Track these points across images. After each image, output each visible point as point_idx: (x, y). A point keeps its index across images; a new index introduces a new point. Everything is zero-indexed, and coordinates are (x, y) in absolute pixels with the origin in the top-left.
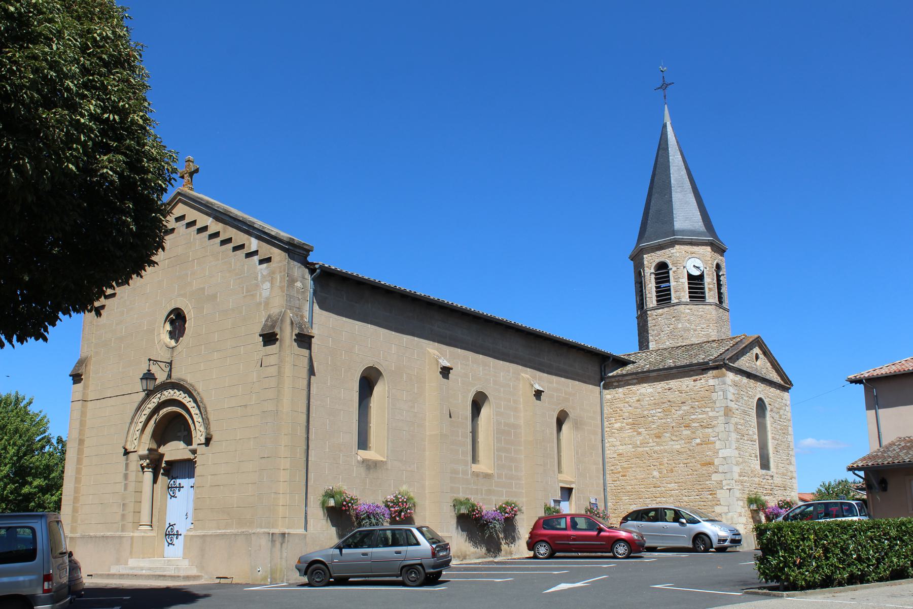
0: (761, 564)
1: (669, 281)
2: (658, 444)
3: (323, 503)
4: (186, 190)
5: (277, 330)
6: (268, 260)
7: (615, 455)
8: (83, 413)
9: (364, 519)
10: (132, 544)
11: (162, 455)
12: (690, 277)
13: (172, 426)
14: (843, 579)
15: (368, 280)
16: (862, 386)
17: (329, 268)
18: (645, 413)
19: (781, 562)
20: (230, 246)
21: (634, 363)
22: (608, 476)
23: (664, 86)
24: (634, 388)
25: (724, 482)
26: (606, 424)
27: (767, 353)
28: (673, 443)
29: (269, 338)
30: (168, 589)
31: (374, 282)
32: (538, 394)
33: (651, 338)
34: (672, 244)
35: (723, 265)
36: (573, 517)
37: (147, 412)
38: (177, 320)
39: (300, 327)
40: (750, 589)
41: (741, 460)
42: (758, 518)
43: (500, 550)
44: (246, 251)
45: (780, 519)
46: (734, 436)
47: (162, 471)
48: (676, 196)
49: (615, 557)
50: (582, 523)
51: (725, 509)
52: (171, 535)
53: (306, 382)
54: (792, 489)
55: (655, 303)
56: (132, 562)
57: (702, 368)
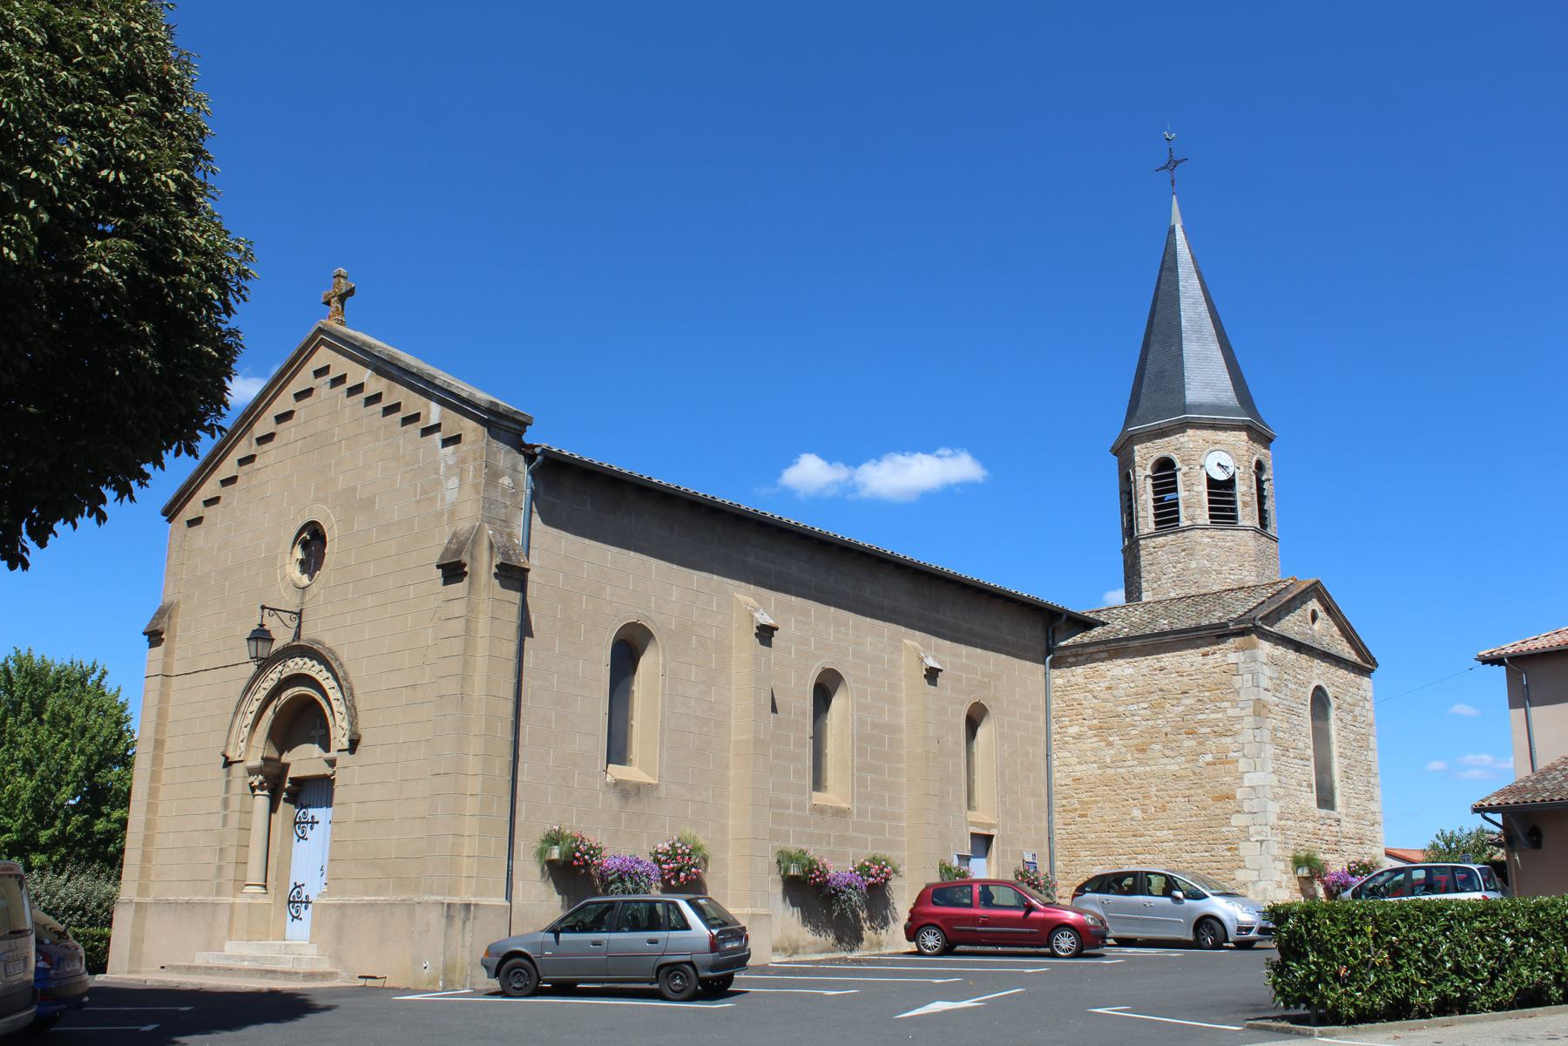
0: (1279, 975)
1: (1175, 490)
2: (1141, 763)
3: (542, 853)
4: (333, 325)
5: (465, 558)
6: (455, 440)
8: (163, 697)
9: (612, 882)
10: (231, 917)
11: (286, 767)
12: (1212, 483)
13: (300, 720)
14: (1427, 1005)
15: (630, 476)
16: (1503, 668)
17: (559, 454)
18: (1121, 709)
19: (1311, 972)
20: (398, 416)
21: (1104, 624)
22: (1056, 816)
23: (1172, 164)
24: (1102, 666)
25: (1252, 830)
26: (1054, 727)
27: (1331, 609)
28: (1165, 761)
29: (453, 571)
30: (274, 994)
31: (640, 479)
32: (932, 675)
33: (1144, 585)
34: (1182, 427)
35: (1268, 464)
36: (986, 885)
37: (261, 695)
38: (313, 540)
39: (506, 554)
40: (1257, 1017)
41: (1282, 791)
42: (1311, 891)
43: (860, 939)
44: (422, 424)
45: (1349, 893)
46: (1270, 750)
47: (284, 795)
48: (1189, 348)
49: (1053, 955)
50: (1002, 896)
51: (1253, 875)
52: (296, 902)
53: (512, 648)
54: (1373, 842)
55: (1152, 526)
56: (231, 948)
57: (1218, 634)
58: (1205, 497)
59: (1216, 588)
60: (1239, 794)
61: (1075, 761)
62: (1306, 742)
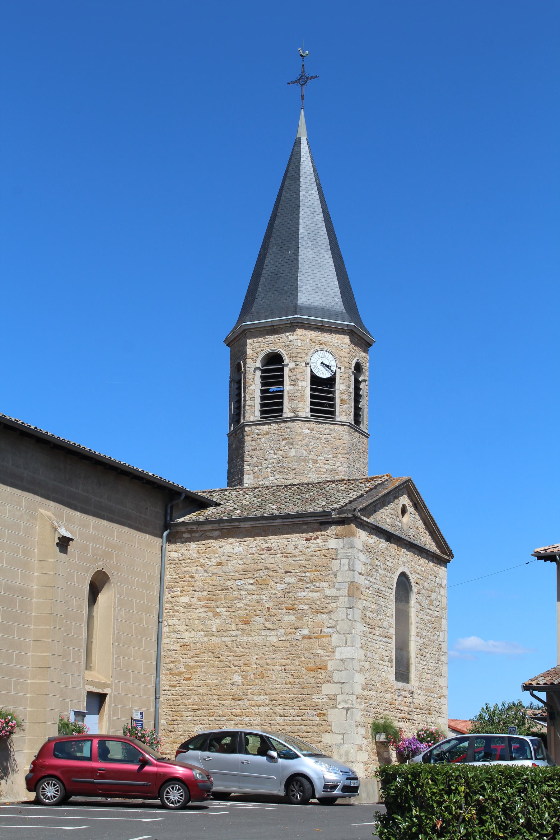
0: (385, 826)
1: (281, 383)
2: (244, 633)
7: (177, 646)
12: (315, 380)
16: (554, 564)
18: (229, 583)
19: (413, 824)
21: (217, 504)
22: (163, 678)
23: (303, 80)
24: (215, 544)
25: (340, 698)
26: (167, 596)
27: (419, 505)
28: (267, 632)
32: (64, 543)
33: (247, 468)
34: (292, 326)
35: (366, 366)
36: (103, 740)
41: (367, 665)
42: (385, 755)
45: (419, 758)
46: (359, 628)
49: (163, 806)
50: (116, 750)
51: (338, 739)
55: (258, 414)
57: (321, 521)
58: (308, 392)
59: (314, 478)
60: (331, 665)
61: (184, 629)
62: (389, 622)
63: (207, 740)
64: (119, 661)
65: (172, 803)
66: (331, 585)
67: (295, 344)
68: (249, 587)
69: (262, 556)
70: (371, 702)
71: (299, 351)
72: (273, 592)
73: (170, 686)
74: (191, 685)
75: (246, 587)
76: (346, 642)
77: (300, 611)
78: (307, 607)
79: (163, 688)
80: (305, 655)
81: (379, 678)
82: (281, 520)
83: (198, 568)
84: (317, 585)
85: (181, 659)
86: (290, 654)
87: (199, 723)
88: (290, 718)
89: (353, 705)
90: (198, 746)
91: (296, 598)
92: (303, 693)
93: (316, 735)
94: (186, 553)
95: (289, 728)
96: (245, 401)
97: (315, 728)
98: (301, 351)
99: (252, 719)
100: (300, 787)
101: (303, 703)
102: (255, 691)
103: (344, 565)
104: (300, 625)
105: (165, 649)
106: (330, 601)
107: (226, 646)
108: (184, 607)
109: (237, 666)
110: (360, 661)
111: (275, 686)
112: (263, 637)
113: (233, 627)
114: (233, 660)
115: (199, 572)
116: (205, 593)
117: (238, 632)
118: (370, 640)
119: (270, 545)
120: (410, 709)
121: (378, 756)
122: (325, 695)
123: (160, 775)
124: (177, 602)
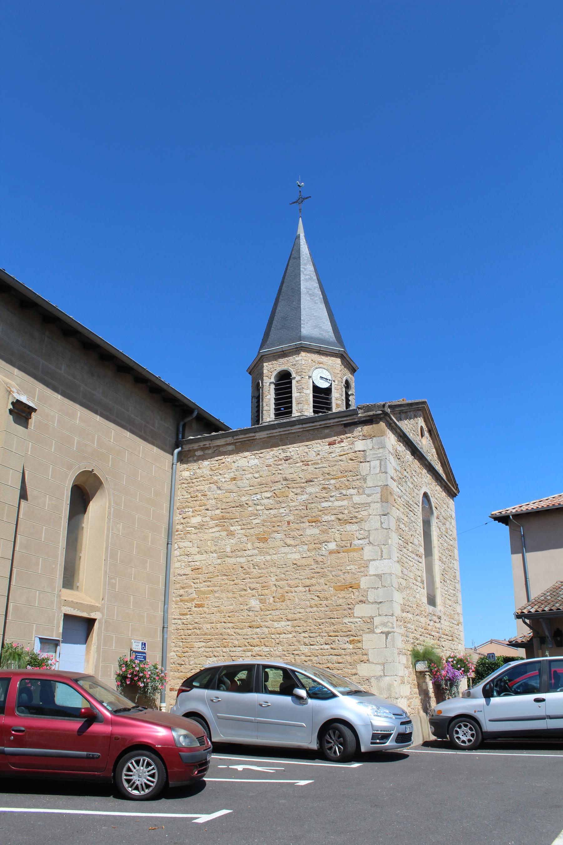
2: (261, 552)
7: (188, 571)
12: (316, 389)
18: (244, 499)
24: (229, 459)
25: (377, 621)
26: (177, 518)
28: (287, 549)
34: (298, 350)
35: (353, 385)
41: (404, 582)
51: (378, 670)
55: (273, 416)
60: (364, 583)
61: (195, 551)
63: (216, 675)
64: (114, 581)
65: (137, 788)
66: (361, 491)
67: (300, 363)
68: (265, 501)
69: (280, 467)
70: (409, 625)
71: (303, 367)
72: (293, 504)
73: (181, 614)
74: (203, 612)
75: (262, 501)
76: (382, 554)
77: (324, 523)
78: (333, 518)
79: (173, 616)
80: (333, 573)
81: (414, 600)
82: (300, 426)
83: (211, 485)
84: (344, 492)
85: (192, 584)
86: (315, 573)
87: (212, 655)
88: (317, 647)
89: (393, 628)
90: (205, 681)
91: (320, 508)
92: (332, 616)
93: (349, 667)
94: (198, 471)
95: (316, 658)
96: (263, 407)
97: (348, 658)
98: (304, 368)
99: (272, 650)
100: (339, 737)
101: (332, 628)
102: (275, 617)
103: (374, 468)
104: (325, 539)
105: (176, 574)
106: (360, 509)
107: (242, 567)
108: (195, 528)
109: (254, 589)
110: (398, 577)
111: (298, 610)
112: (283, 555)
113: (249, 546)
114: (250, 583)
115: (212, 490)
116: (218, 512)
117: (254, 551)
118: (405, 555)
119: (288, 454)
120: (439, 635)
121: (418, 688)
122: (359, 618)
123: (117, 739)
124: (188, 523)
